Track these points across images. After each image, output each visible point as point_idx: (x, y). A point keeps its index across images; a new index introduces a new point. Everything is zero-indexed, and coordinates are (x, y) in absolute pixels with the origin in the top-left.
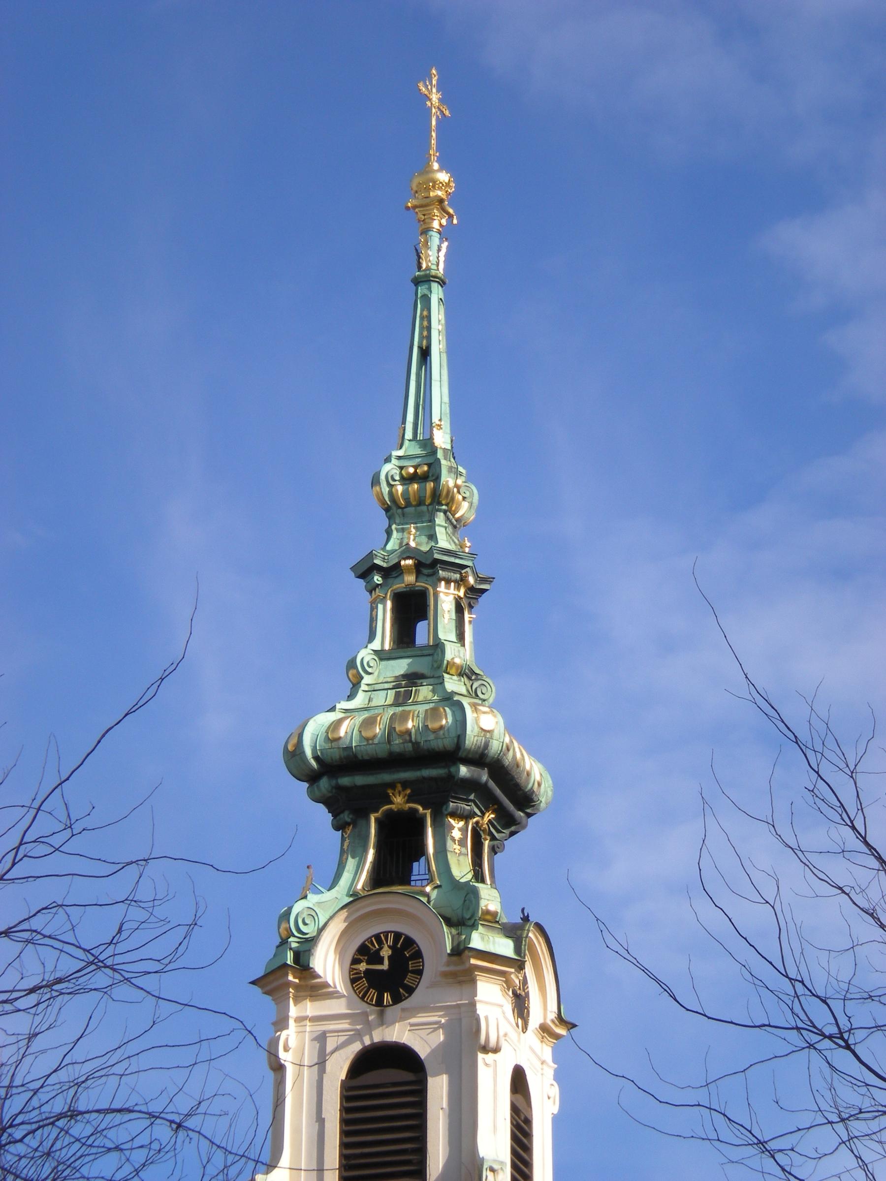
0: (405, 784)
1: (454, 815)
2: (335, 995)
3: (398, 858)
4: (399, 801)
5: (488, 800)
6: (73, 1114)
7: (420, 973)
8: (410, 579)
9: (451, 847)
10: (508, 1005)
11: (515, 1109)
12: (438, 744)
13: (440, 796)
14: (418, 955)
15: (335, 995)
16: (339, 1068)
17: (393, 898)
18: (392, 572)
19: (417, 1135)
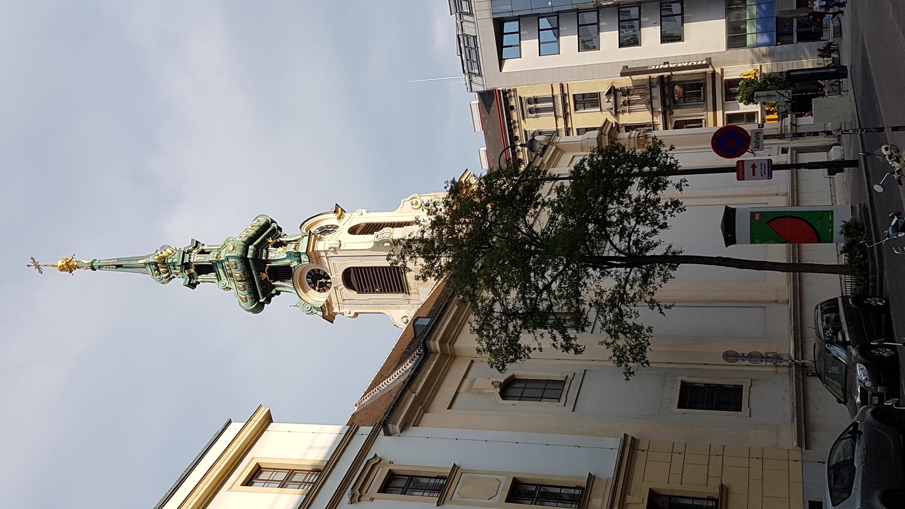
0: (258, 274)
1: (267, 257)
2: (330, 297)
3: (284, 273)
4: (264, 276)
5: (264, 244)
6: (815, 362)
7: (319, 270)
8: (192, 271)
9: (277, 255)
10: (328, 237)
11: (362, 233)
12: (263, 225)
13: (260, 263)
14: (313, 270)
15: (330, 297)
16: (353, 294)
17: (296, 275)
18: (191, 276)
19: (554, 148)
